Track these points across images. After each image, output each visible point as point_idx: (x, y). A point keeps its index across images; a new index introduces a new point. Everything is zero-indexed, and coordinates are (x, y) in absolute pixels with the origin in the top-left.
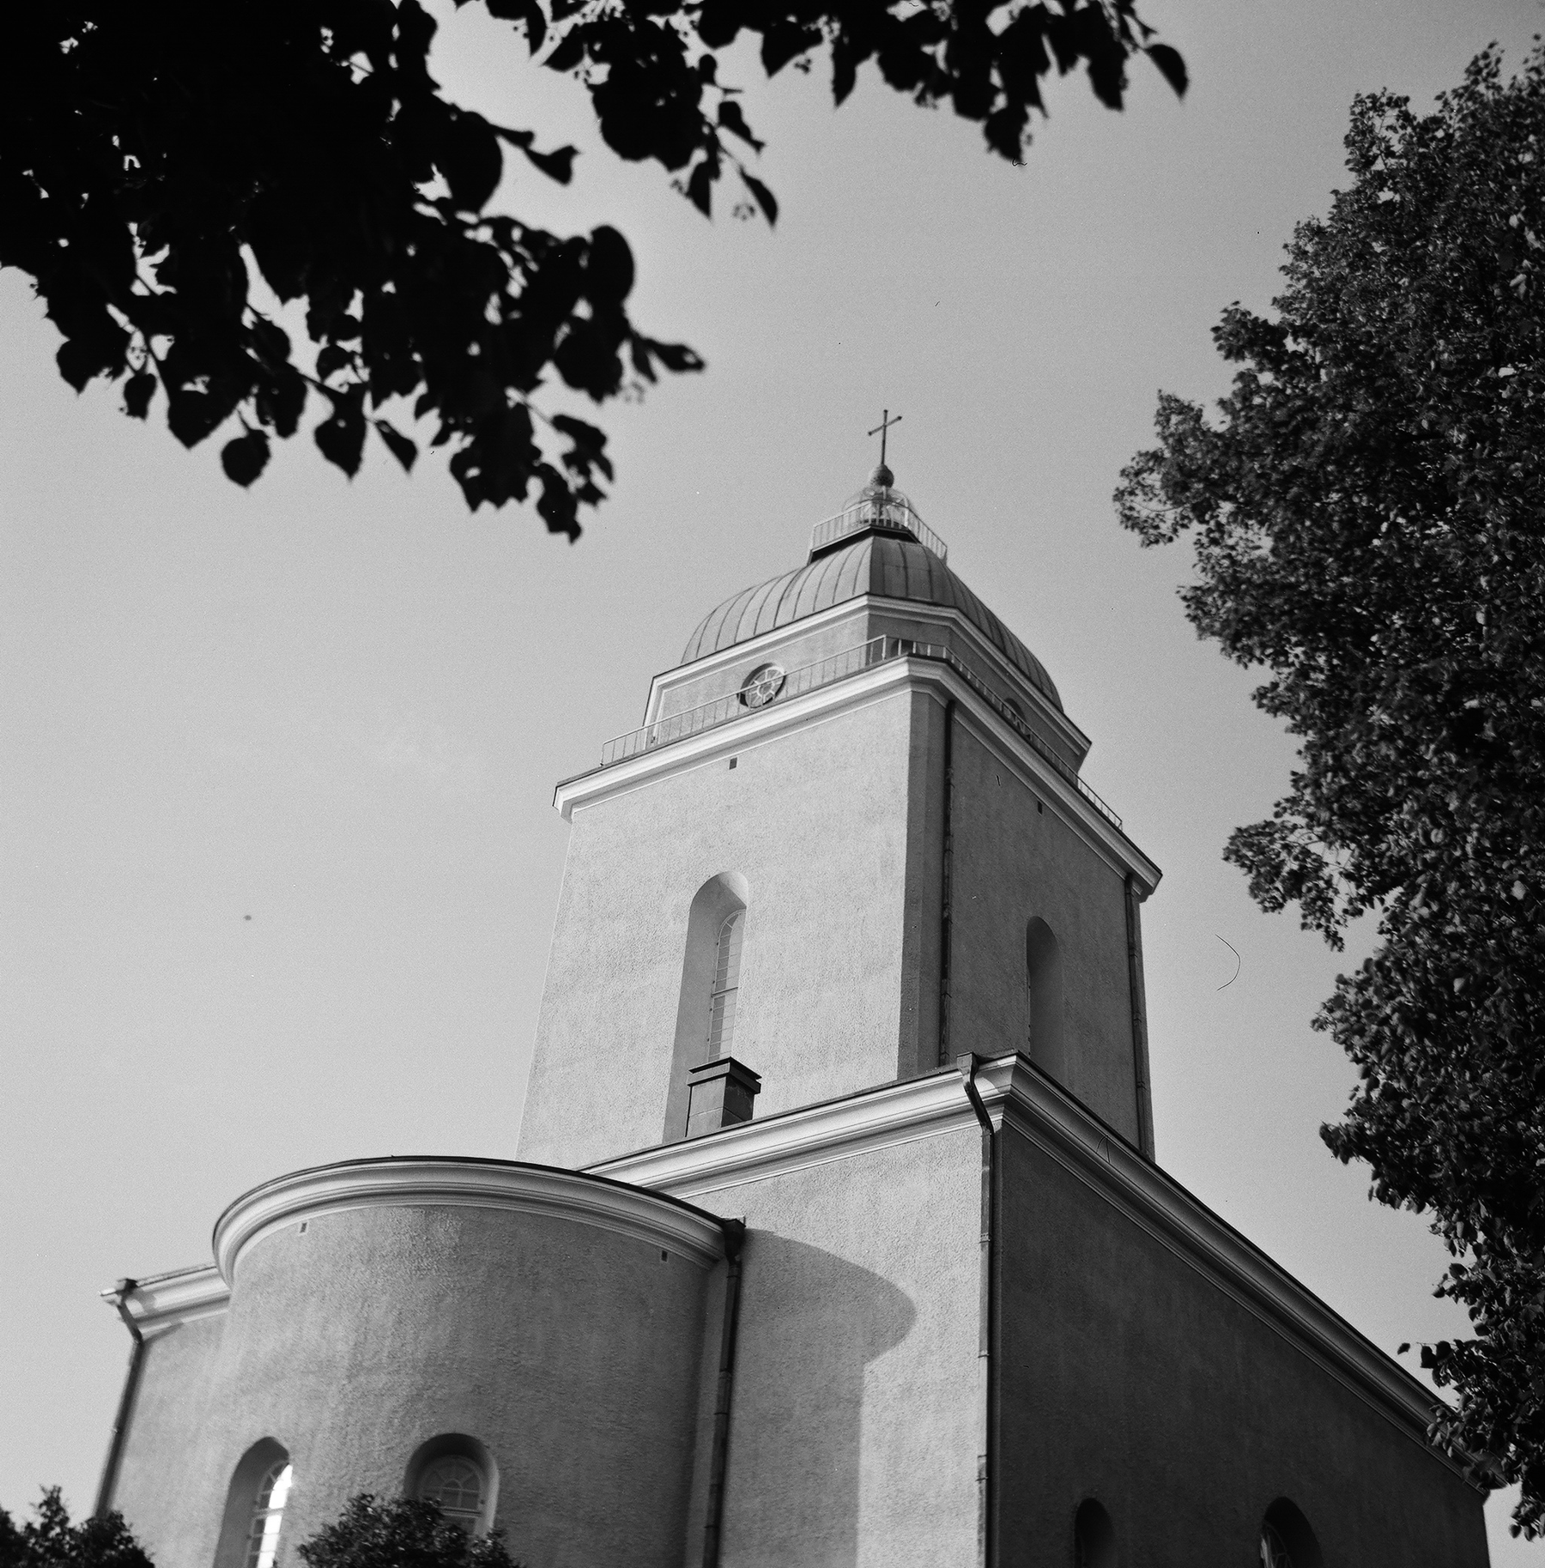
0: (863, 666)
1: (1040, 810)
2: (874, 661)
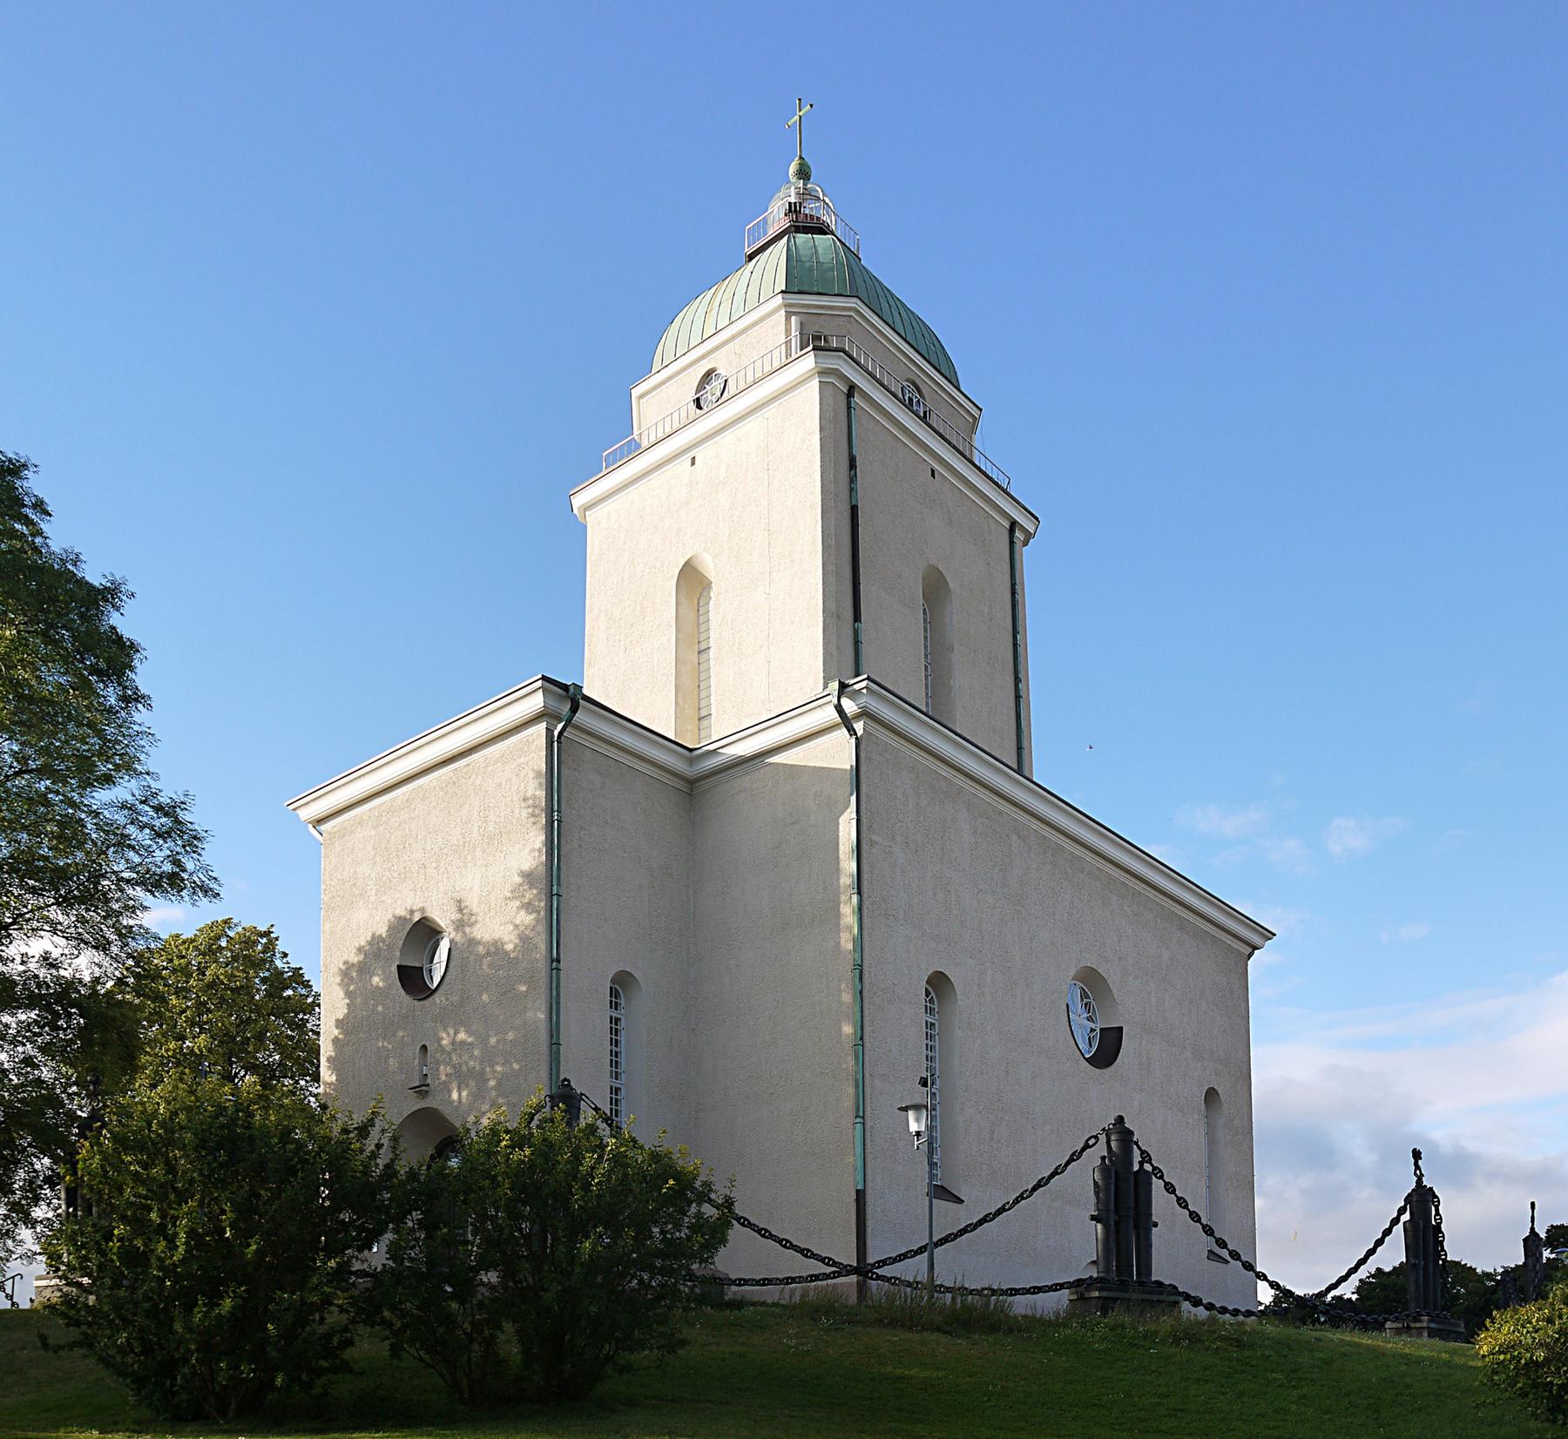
1: (933, 475)
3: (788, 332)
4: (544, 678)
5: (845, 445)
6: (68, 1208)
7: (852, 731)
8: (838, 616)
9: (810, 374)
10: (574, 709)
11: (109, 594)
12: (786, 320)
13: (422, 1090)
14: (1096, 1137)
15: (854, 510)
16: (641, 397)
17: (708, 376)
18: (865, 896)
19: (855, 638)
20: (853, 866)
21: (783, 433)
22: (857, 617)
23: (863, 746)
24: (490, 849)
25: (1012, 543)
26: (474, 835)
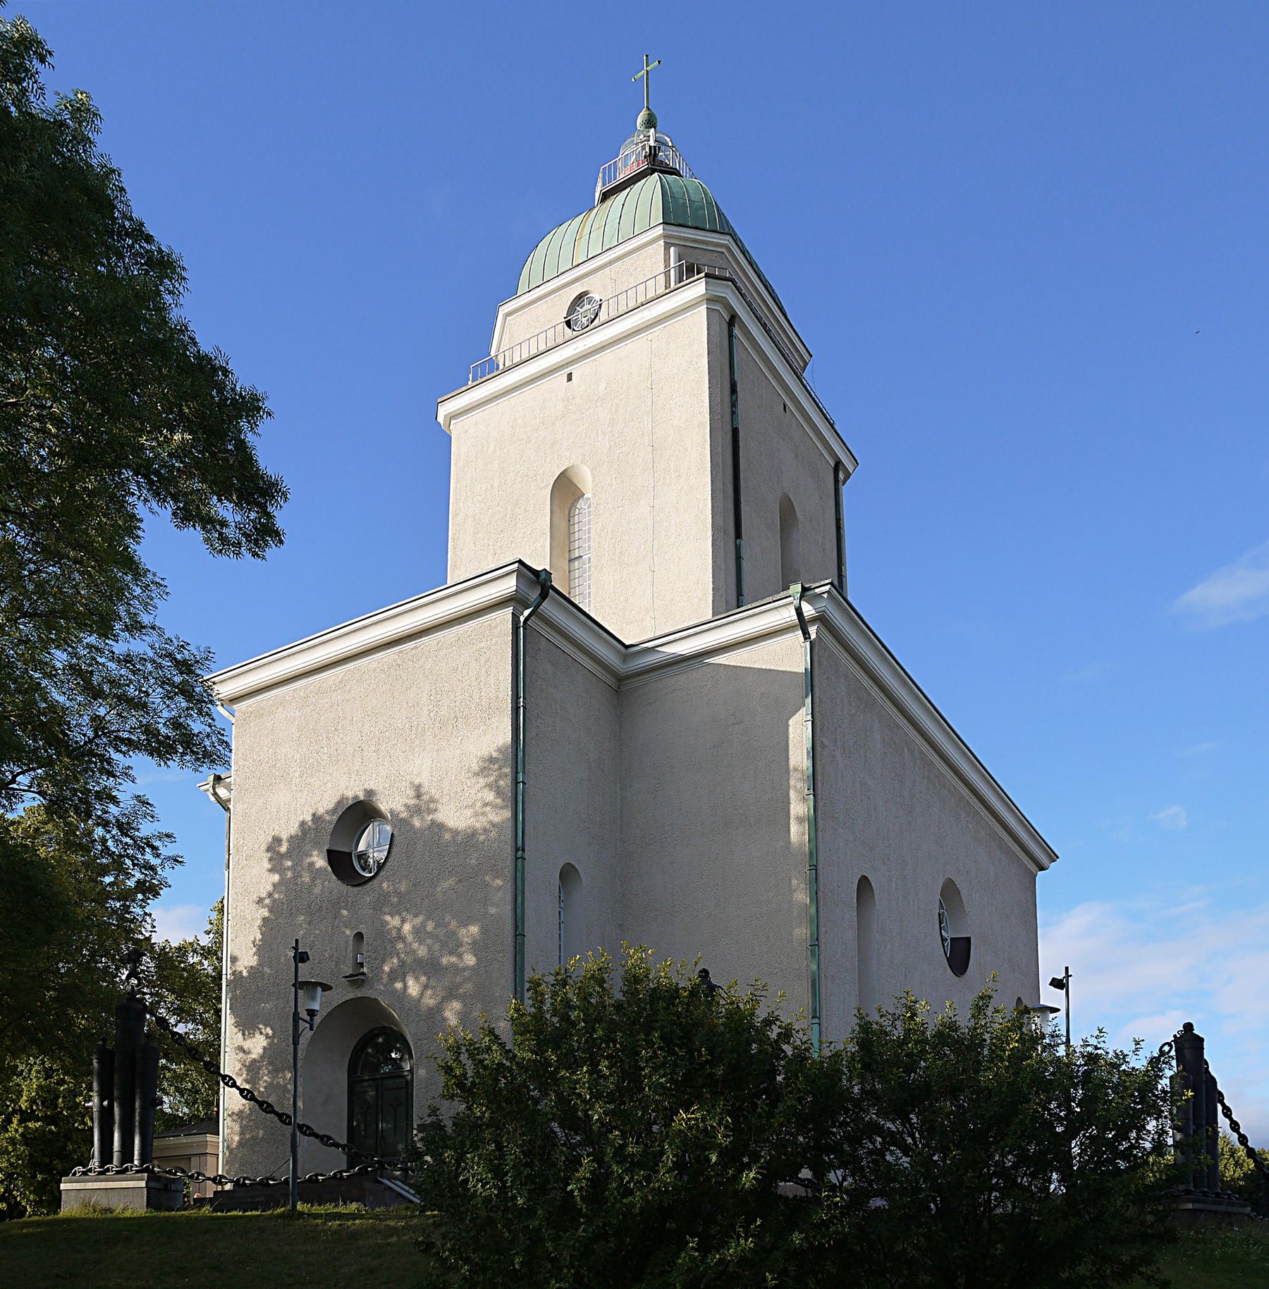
0: (661, 290)
2: (473, 381)
3: (667, 261)
4: (520, 562)
5: (727, 371)
6: (101, 1101)
7: (806, 634)
8: (725, 533)
9: (700, 300)
10: (544, 596)
11: (250, 407)
12: (665, 250)
13: (357, 979)
14: (1169, 1044)
15: (735, 433)
16: (508, 314)
17: (580, 299)
18: (819, 797)
19: (736, 554)
20: (806, 764)
21: (668, 354)
22: (738, 535)
23: (816, 651)
24: (444, 733)
25: (836, 481)
26: (423, 719)
